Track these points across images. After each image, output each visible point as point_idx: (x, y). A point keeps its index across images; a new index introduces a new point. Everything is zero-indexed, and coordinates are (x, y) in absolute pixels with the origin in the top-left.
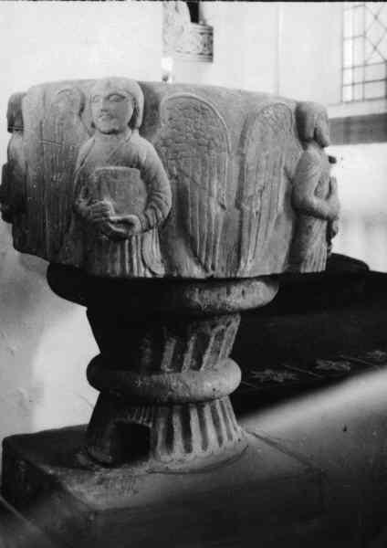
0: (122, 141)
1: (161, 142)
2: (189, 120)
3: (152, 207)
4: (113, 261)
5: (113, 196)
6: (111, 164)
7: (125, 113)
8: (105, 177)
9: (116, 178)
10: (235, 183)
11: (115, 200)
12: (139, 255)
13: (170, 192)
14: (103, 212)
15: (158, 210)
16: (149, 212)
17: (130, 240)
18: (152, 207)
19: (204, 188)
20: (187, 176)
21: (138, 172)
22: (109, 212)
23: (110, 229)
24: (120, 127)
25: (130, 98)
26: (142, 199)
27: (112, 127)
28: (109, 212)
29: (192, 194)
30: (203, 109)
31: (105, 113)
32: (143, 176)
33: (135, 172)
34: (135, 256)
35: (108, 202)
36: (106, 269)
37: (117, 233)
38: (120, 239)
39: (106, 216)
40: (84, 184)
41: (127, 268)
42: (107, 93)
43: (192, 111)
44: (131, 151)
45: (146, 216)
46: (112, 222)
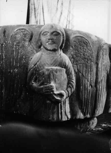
0: (58, 55)
1: (71, 56)
2: (82, 47)
3: (70, 87)
4: (53, 113)
5: (55, 81)
6: (53, 66)
7: (60, 41)
8: (52, 73)
9: (56, 72)
10: (95, 77)
11: (56, 83)
12: (64, 110)
13: (75, 80)
14: (51, 89)
15: (72, 88)
16: (69, 89)
17: (61, 103)
18: (70, 87)
19: (86, 78)
20: (81, 73)
21: (65, 70)
22: (54, 90)
23: (54, 98)
24: (41, 49)
25: (62, 34)
26: (66, 83)
27: (54, 47)
28: (54, 90)
29: (82, 81)
30: (86, 43)
31: (50, 41)
32: (66, 72)
33: (64, 70)
34: (63, 111)
35: (53, 84)
36: (49, 117)
37: (57, 99)
38: (58, 102)
39: (53, 91)
40: (35, 75)
41: (60, 117)
42: (52, 31)
43: (83, 43)
44: (62, 60)
45: (68, 91)
46: (55, 95)
